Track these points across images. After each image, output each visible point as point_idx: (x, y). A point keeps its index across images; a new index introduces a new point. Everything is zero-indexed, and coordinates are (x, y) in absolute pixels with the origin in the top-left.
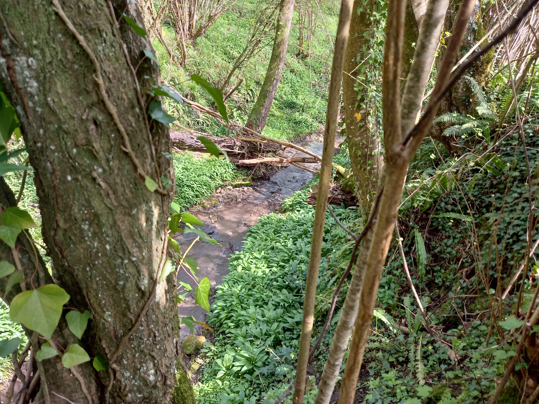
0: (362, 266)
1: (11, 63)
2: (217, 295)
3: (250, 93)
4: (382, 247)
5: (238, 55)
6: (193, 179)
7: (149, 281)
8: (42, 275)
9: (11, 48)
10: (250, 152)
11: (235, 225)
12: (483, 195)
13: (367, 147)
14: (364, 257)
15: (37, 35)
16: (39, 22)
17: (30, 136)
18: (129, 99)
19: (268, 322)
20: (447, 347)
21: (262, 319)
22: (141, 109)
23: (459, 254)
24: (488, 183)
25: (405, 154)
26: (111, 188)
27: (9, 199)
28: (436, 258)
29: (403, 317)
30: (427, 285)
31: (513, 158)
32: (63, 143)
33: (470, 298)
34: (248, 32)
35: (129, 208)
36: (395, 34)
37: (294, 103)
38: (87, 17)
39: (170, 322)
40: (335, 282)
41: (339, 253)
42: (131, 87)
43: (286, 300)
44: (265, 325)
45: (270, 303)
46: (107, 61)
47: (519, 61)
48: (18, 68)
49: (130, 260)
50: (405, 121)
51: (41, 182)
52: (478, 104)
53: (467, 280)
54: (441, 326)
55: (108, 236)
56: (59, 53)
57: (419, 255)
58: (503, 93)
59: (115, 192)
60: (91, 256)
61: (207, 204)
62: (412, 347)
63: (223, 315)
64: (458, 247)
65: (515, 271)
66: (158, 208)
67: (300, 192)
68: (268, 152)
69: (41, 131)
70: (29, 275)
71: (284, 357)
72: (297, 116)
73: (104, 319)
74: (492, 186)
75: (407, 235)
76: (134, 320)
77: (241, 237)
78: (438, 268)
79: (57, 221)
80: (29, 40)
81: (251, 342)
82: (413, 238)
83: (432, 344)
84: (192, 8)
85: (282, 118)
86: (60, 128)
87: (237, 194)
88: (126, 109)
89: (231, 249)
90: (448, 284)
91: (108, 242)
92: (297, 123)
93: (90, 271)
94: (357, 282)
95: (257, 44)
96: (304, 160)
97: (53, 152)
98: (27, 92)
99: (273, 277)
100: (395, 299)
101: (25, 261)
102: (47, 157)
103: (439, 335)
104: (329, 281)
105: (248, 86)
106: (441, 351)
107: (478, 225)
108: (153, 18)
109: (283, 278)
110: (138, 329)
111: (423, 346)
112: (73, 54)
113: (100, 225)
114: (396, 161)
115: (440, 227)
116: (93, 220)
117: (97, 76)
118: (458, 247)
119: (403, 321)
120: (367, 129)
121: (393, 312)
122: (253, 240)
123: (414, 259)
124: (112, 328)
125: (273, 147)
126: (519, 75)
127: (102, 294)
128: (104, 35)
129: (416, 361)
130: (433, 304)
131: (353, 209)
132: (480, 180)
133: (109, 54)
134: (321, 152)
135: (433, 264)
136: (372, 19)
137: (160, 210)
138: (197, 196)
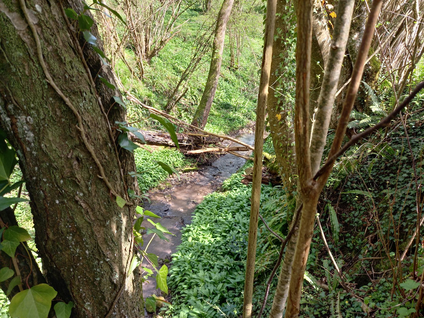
0: (289, 262)
1: (14, 120)
2: (172, 262)
3: (194, 98)
4: (303, 256)
5: (184, 70)
6: (151, 167)
7: (120, 275)
8: (35, 274)
9: (14, 110)
10: (195, 144)
11: (185, 203)
12: (380, 175)
13: (287, 140)
14: (290, 256)
15: (34, 100)
16: (36, 91)
17: (27, 172)
18: (103, 138)
19: (215, 283)
20: (360, 301)
21: (210, 281)
22: (112, 143)
23: (365, 223)
24: (383, 165)
25: (316, 187)
26: (90, 207)
27: (9, 217)
28: (346, 227)
29: (324, 276)
30: (341, 249)
31: (401, 146)
32: (53, 176)
33: (376, 260)
34: (191, 52)
35: (104, 222)
36: (303, 102)
37: (228, 104)
38: (72, 84)
39: (137, 305)
40: (267, 248)
41: (269, 224)
42: (105, 129)
43: (228, 263)
44: (212, 285)
45: (215, 267)
46: (86, 113)
47: (399, 70)
48: (19, 124)
49: (104, 261)
50: (314, 154)
51: (35, 204)
52: (371, 104)
53: (372, 245)
54: (354, 284)
55: (87, 244)
56: (51, 112)
57: (333, 225)
58: (390, 95)
59: (93, 210)
60: (74, 260)
61: (163, 187)
62: (332, 302)
63: (178, 279)
64: (363, 218)
65: (410, 237)
66: (126, 217)
67: (236, 174)
68: (210, 143)
69: (36, 168)
70: (25, 276)
71: (229, 313)
72: (231, 114)
73: (85, 308)
74: (386, 168)
75: (322, 208)
76: (108, 308)
77: (190, 213)
78: (348, 235)
79: (47, 234)
80: (27, 104)
81: (201, 300)
82: (328, 210)
83: (348, 299)
84: (148, 35)
85: (219, 116)
86: (51, 165)
87: (186, 178)
88: (101, 146)
89: (183, 223)
90: (357, 247)
91: (87, 249)
92: (232, 120)
93: (73, 271)
94: (285, 275)
95: (198, 61)
96: (238, 149)
97: (45, 183)
98: (25, 141)
99: (217, 245)
100: (316, 261)
101: (22, 264)
102: (41, 187)
103: (353, 291)
104: (263, 247)
105: (192, 93)
106: (355, 305)
107: (377, 200)
108: (117, 44)
109: (225, 246)
110: (112, 315)
111: (341, 301)
112: (61, 111)
113: (81, 236)
114: (309, 193)
115: (348, 202)
116: (76, 232)
117: (79, 126)
118: (363, 218)
119: (324, 279)
120: (286, 126)
121: (315, 272)
122: (201, 215)
123: (329, 227)
124: (91, 315)
125: (213, 140)
126: (401, 80)
127: (83, 289)
128: (85, 95)
129: (336, 313)
130: (347, 264)
131: (278, 188)
132: (377, 163)
133: (87, 107)
134: (252, 142)
135: (344, 232)
136: (285, 43)
137: (127, 218)
138: (154, 181)
